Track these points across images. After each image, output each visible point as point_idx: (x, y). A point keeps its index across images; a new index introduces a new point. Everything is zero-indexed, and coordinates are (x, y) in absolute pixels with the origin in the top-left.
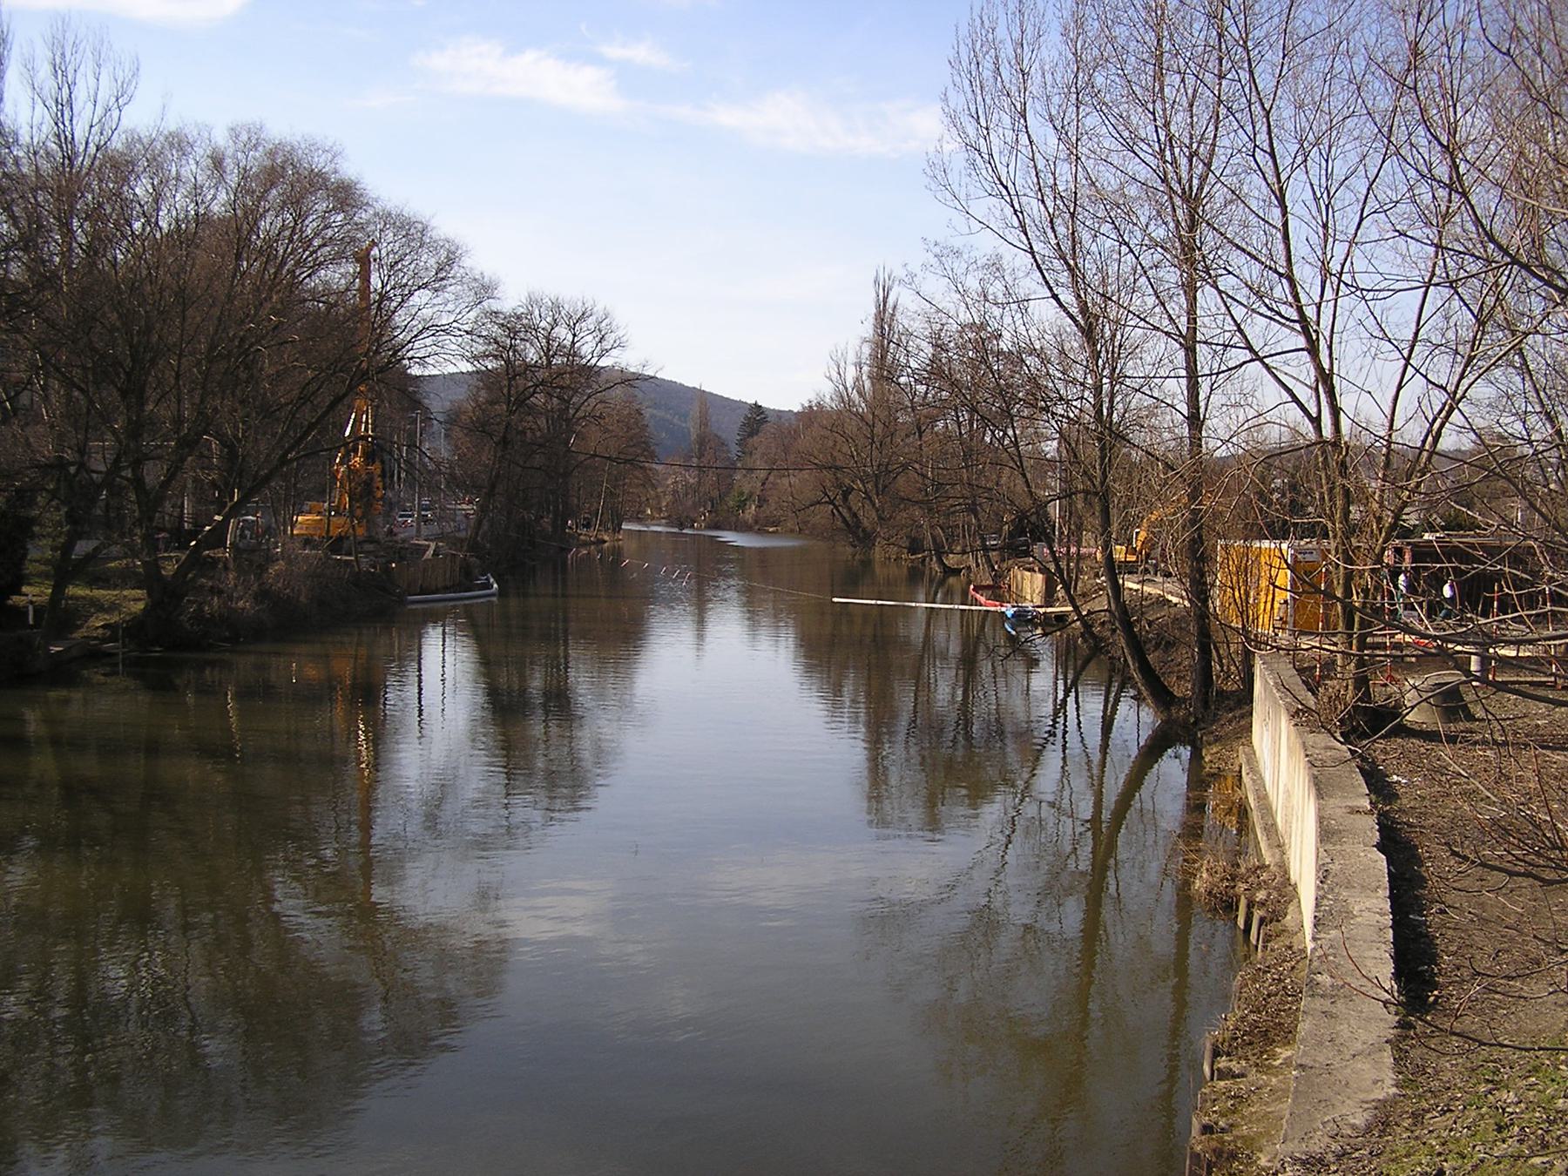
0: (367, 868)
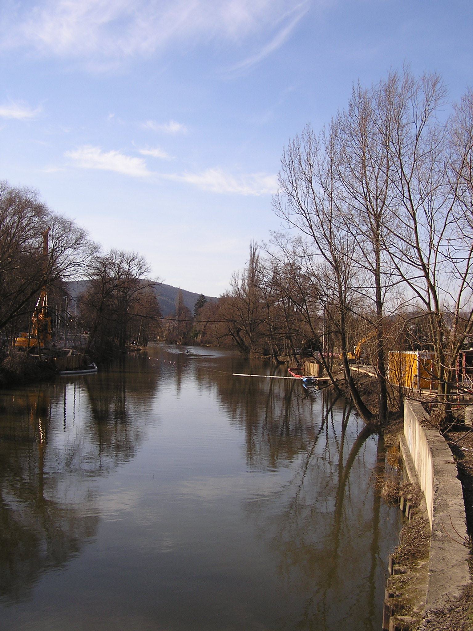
0: (42, 482)
